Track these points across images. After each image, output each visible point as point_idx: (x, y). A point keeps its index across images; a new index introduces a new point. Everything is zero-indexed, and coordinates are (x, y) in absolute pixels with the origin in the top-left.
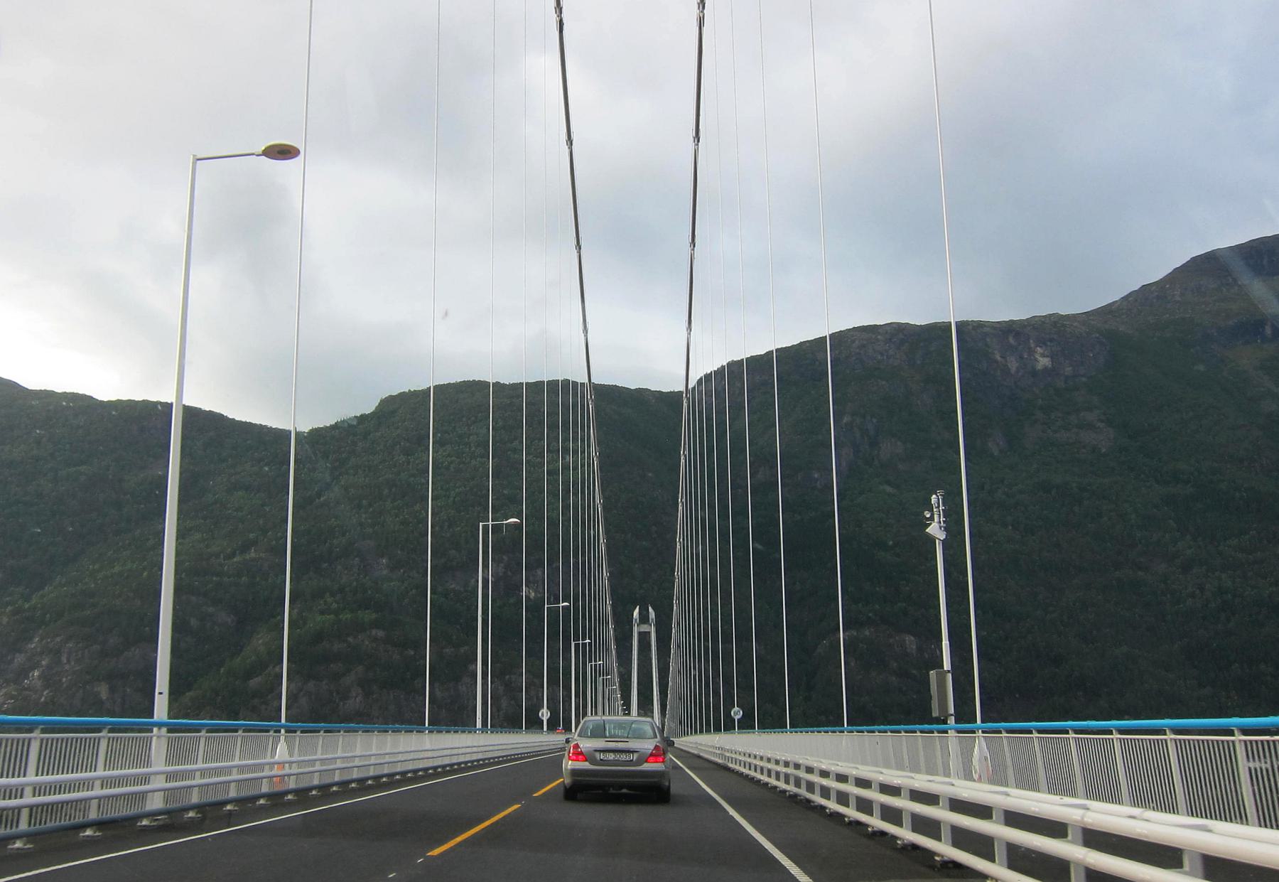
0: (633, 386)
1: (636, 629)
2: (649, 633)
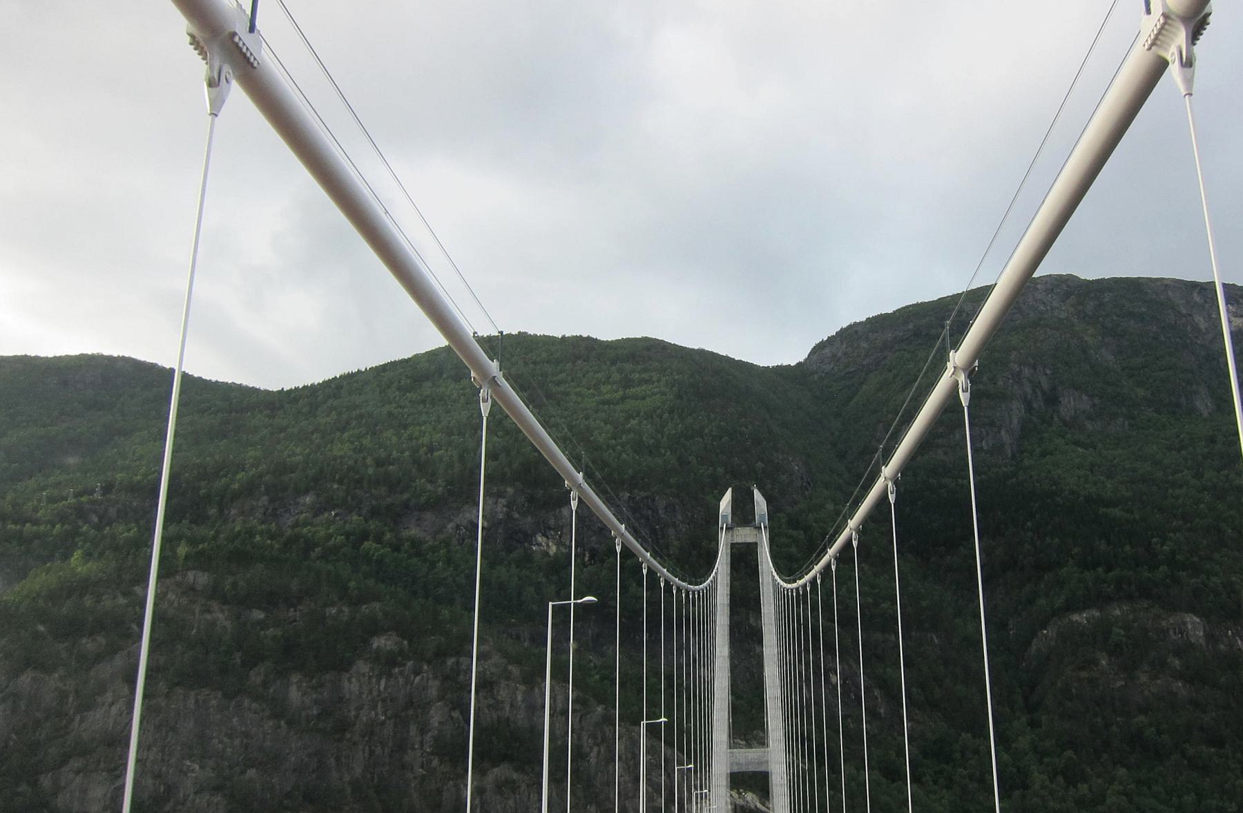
1: (723, 539)
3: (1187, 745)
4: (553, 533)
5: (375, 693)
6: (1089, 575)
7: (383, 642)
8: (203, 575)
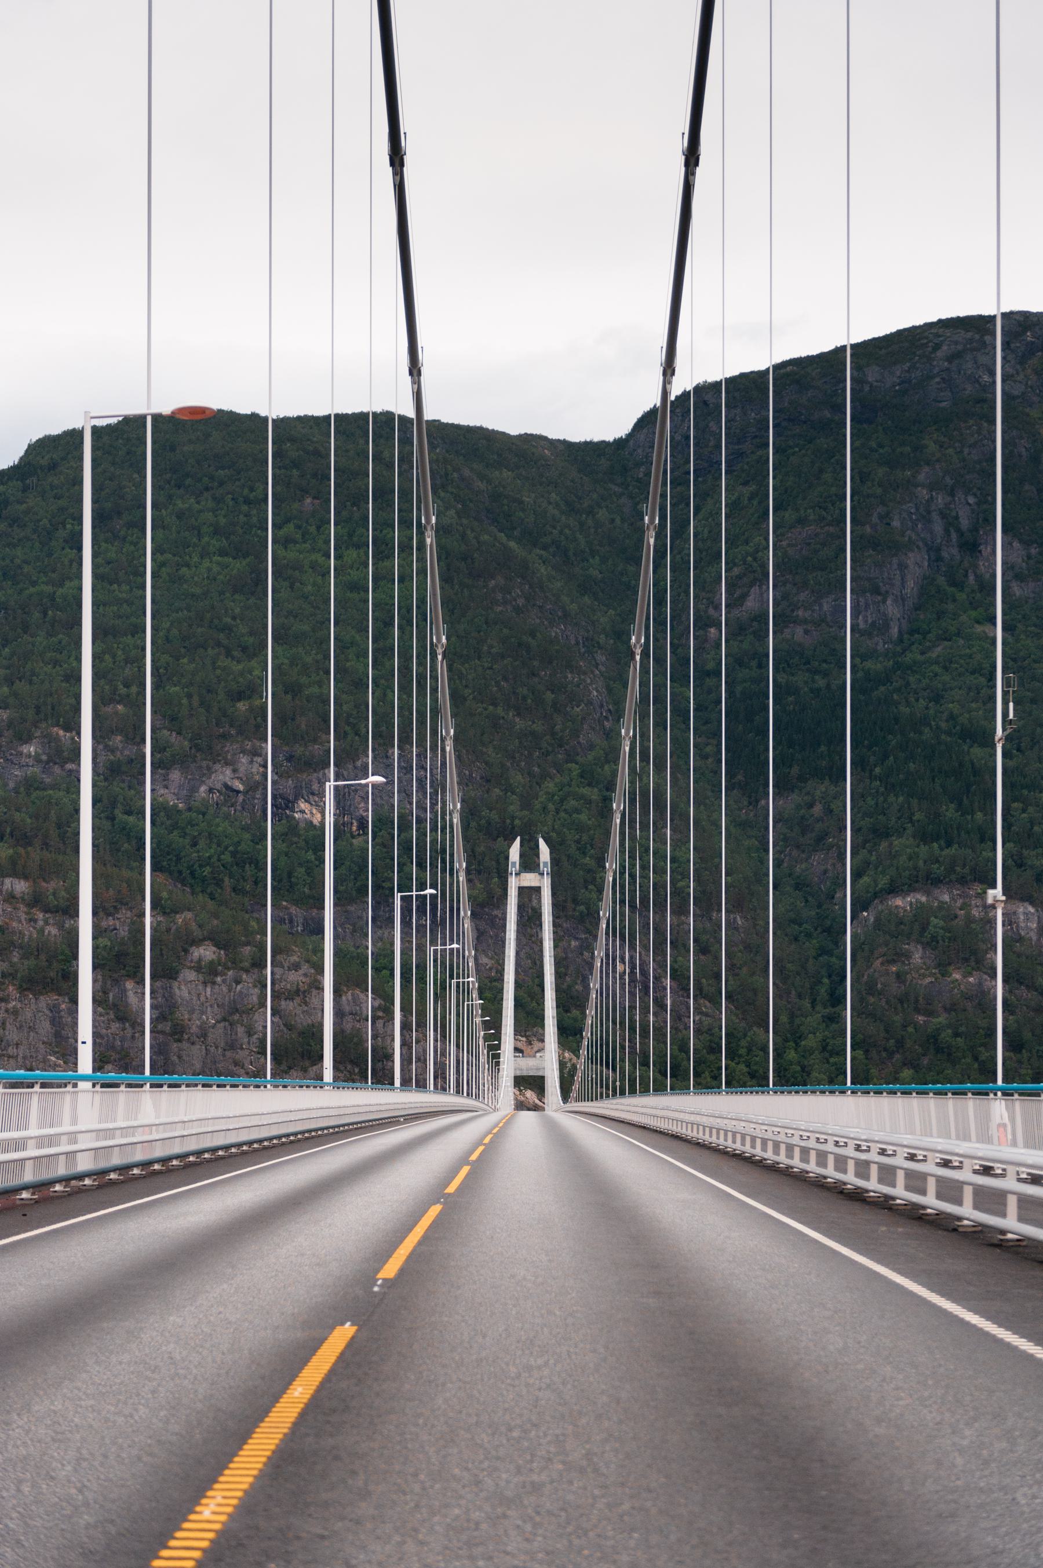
0: (514, 429)
2: (538, 890)
3: (982, 1049)
4: (317, 799)
5: (202, 998)
6: (924, 849)
7: (206, 952)
8: (20, 882)
